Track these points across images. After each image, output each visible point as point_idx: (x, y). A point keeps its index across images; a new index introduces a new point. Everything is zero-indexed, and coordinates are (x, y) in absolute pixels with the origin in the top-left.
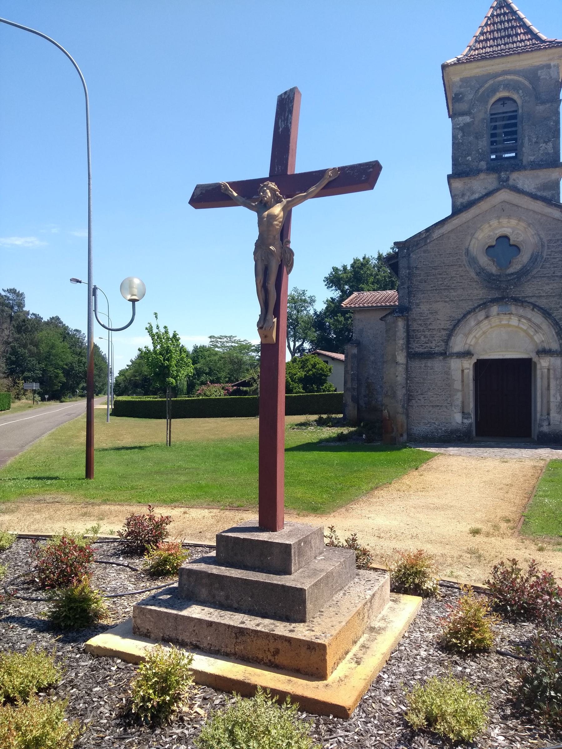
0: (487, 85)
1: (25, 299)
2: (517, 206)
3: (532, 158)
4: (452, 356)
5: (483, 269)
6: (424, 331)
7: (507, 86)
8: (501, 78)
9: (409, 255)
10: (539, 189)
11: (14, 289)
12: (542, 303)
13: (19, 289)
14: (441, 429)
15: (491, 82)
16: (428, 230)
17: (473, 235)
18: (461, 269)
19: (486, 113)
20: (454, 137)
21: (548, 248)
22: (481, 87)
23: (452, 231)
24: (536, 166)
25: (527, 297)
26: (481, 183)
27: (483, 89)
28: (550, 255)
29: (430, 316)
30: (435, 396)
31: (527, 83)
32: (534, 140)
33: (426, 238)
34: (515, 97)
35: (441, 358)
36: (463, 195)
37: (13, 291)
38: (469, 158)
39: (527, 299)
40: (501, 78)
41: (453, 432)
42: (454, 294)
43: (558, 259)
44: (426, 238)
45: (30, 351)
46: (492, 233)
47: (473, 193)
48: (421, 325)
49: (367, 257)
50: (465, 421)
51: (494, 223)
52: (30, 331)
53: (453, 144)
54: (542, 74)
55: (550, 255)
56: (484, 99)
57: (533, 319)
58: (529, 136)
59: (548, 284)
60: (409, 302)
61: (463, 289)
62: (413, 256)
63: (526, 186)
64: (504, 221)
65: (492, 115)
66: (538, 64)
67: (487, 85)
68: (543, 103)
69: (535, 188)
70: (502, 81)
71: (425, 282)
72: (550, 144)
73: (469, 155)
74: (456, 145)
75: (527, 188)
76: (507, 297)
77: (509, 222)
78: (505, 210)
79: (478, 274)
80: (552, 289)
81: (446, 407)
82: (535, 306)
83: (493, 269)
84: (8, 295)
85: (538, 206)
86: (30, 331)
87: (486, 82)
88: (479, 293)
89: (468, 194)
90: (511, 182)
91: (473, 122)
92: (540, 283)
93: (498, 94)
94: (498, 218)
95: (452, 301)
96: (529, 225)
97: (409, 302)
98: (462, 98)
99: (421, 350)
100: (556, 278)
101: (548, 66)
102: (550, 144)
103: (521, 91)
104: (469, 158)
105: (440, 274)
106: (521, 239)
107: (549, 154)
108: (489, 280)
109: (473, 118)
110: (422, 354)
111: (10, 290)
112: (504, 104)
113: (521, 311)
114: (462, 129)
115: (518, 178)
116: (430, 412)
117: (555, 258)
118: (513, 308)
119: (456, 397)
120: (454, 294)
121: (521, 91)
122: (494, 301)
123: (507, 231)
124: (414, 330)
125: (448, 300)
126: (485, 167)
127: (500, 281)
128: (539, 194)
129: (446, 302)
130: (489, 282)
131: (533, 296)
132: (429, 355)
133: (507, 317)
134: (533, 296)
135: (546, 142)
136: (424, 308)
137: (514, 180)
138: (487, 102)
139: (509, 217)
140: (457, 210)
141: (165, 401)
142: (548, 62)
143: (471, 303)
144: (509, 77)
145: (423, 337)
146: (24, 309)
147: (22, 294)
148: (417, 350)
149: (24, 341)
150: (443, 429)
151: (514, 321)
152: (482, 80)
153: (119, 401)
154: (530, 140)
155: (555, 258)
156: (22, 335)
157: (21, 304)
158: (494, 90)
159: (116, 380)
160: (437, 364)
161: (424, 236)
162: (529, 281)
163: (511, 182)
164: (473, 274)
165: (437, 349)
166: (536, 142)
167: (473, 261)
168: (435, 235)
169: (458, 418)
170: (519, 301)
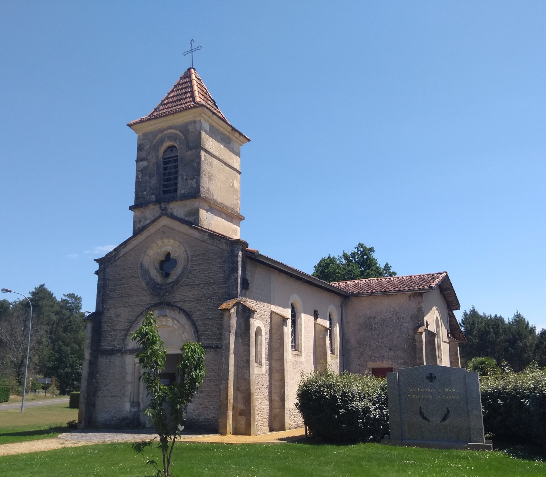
0: (157, 138)
1: (82, 303)
2: (174, 230)
3: (183, 192)
4: (126, 353)
5: (151, 279)
6: (111, 332)
7: (172, 137)
8: (166, 132)
9: (105, 269)
10: (186, 216)
11: (73, 294)
12: (186, 306)
13: (77, 294)
14: (116, 417)
15: (160, 135)
16: (115, 250)
17: (145, 252)
18: (136, 280)
19: (157, 157)
20: (137, 177)
21: (191, 262)
22: (155, 139)
23: (132, 249)
24: (185, 197)
25: (176, 302)
26: (152, 211)
27: (155, 141)
28: (192, 267)
29: (115, 319)
30: (114, 387)
31: (181, 135)
32: (185, 177)
33: (116, 255)
34: (176, 145)
35: (120, 354)
36: (140, 221)
37: (71, 296)
38: (145, 193)
39: (176, 304)
40: (166, 132)
41: (124, 419)
42: (131, 300)
43: (197, 271)
44: (116, 255)
45: (72, 348)
46: (159, 251)
47: (146, 220)
48: (109, 326)
49: (332, 257)
50: (133, 410)
51: (160, 242)
52: (75, 331)
53: (136, 182)
54: (191, 128)
55: (192, 267)
56: (156, 148)
57: (180, 321)
58: (182, 174)
59: (190, 291)
60: (103, 307)
61: (137, 296)
62: (107, 270)
63: (178, 213)
64: (166, 241)
65: (164, 159)
66: (188, 120)
67: (157, 138)
68: (190, 149)
69: (184, 215)
70: (166, 134)
71: (114, 291)
72: (194, 180)
73: (145, 190)
74: (138, 184)
75: (179, 216)
76: (164, 303)
77: (169, 242)
78: (165, 232)
79: (147, 284)
80: (193, 295)
81: (120, 397)
82: (181, 309)
83: (159, 279)
84: (68, 299)
85: (184, 228)
86: (75, 331)
87: (156, 136)
88: (147, 299)
89: (143, 220)
90: (169, 211)
91: (148, 165)
92: (185, 290)
93: (165, 144)
94: (162, 238)
95: (130, 306)
96: (180, 243)
97: (103, 307)
98: (143, 148)
99: (109, 348)
100: (196, 286)
101: (195, 122)
102: (194, 180)
103: (178, 141)
104: (145, 193)
105: (123, 284)
106: (177, 254)
107: (193, 188)
108: (155, 289)
109: (149, 162)
110: (108, 351)
111: (70, 294)
112: (171, 151)
113: (172, 314)
114: (141, 171)
115: (174, 207)
116: (109, 401)
117: (195, 270)
118: (167, 311)
119: (128, 388)
120: (131, 300)
121: (178, 141)
122: (155, 306)
123: (169, 249)
124: (104, 331)
125: (127, 305)
126: (154, 200)
127: (160, 289)
128: (186, 219)
129: (126, 307)
130: (153, 290)
131: (180, 301)
132: (112, 352)
133: (164, 319)
134: (180, 301)
135: (192, 179)
136: (112, 312)
137: (171, 209)
138: (157, 151)
139: (168, 238)
140: (137, 232)
141: (79, 394)
142: (194, 119)
143: (141, 308)
144: (171, 131)
145: (109, 336)
146: (81, 311)
147: (80, 298)
148: (105, 347)
149: (68, 340)
150: (118, 416)
151: (170, 323)
152: (155, 134)
153: (513, 398)
154: (182, 178)
155: (195, 270)
156: (67, 334)
157: (79, 306)
158: (162, 141)
159: (39, 373)
160: (116, 359)
161: (114, 254)
162: (178, 289)
163: (169, 211)
164: (144, 284)
165: (118, 346)
166: (186, 179)
167: (145, 273)
168: (121, 253)
169: (127, 406)
170: (171, 305)
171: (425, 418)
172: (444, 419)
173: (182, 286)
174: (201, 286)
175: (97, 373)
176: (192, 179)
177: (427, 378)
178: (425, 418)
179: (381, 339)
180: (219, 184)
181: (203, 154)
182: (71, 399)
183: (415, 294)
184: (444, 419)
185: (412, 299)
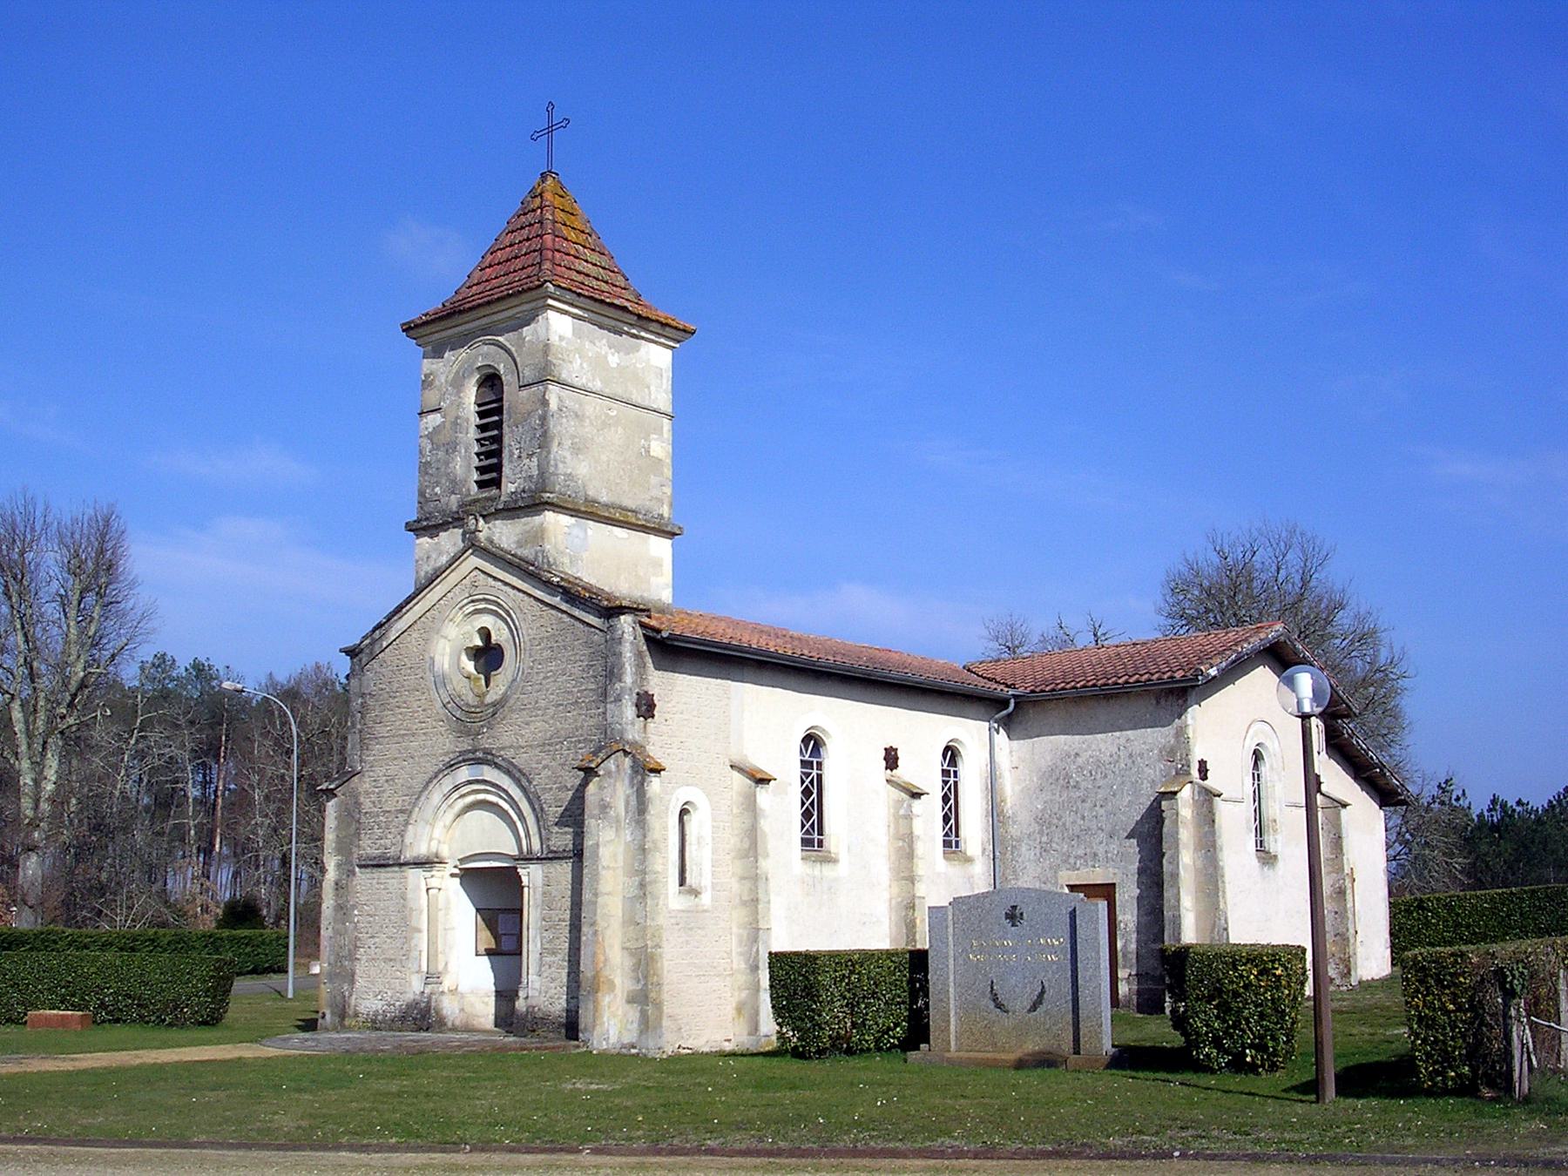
10: (520, 544)
38: (437, 490)
47: (440, 554)
72: (535, 459)
88: (446, 743)
104: (437, 490)
107: (531, 477)
148: (369, 851)
171: (999, 1006)
172: (1034, 1008)
173: (512, 711)
174: (551, 711)
175: (354, 907)
176: (530, 456)
177: (1007, 916)
178: (999, 1006)
179: (1091, 809)
180: (604, 458)
181: (554, 394)
182: (1180, 1049)
183: (1171, 691)
184: (1034, 1008)
185: (1163, 702)
